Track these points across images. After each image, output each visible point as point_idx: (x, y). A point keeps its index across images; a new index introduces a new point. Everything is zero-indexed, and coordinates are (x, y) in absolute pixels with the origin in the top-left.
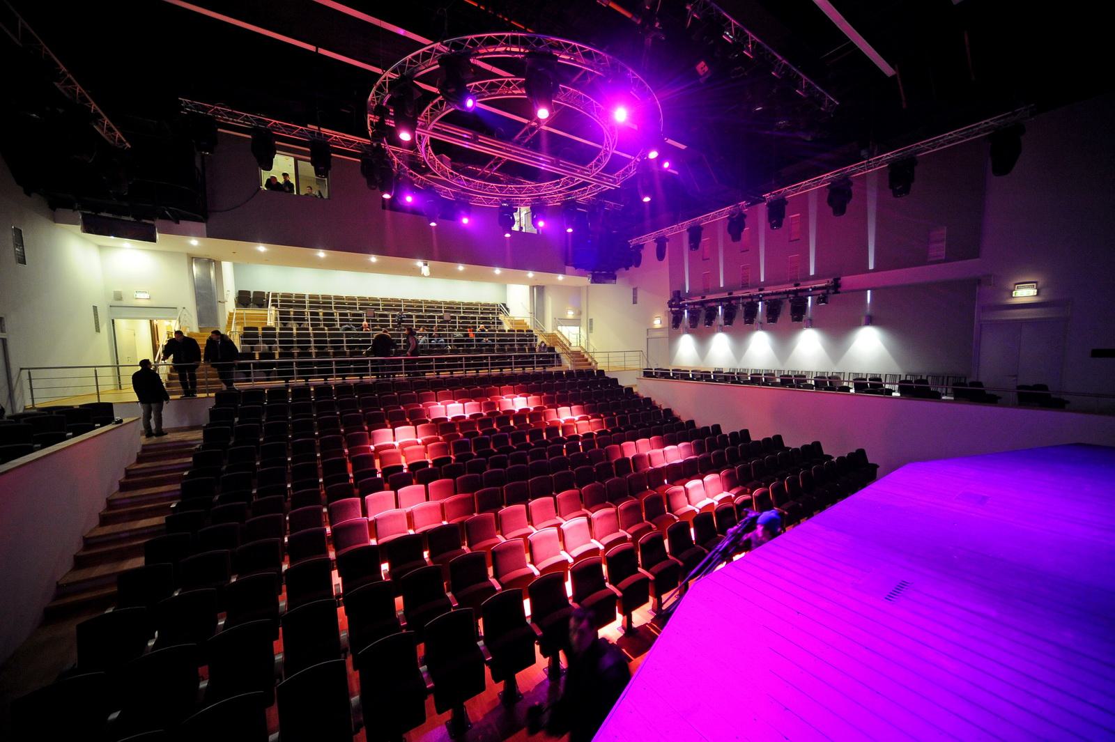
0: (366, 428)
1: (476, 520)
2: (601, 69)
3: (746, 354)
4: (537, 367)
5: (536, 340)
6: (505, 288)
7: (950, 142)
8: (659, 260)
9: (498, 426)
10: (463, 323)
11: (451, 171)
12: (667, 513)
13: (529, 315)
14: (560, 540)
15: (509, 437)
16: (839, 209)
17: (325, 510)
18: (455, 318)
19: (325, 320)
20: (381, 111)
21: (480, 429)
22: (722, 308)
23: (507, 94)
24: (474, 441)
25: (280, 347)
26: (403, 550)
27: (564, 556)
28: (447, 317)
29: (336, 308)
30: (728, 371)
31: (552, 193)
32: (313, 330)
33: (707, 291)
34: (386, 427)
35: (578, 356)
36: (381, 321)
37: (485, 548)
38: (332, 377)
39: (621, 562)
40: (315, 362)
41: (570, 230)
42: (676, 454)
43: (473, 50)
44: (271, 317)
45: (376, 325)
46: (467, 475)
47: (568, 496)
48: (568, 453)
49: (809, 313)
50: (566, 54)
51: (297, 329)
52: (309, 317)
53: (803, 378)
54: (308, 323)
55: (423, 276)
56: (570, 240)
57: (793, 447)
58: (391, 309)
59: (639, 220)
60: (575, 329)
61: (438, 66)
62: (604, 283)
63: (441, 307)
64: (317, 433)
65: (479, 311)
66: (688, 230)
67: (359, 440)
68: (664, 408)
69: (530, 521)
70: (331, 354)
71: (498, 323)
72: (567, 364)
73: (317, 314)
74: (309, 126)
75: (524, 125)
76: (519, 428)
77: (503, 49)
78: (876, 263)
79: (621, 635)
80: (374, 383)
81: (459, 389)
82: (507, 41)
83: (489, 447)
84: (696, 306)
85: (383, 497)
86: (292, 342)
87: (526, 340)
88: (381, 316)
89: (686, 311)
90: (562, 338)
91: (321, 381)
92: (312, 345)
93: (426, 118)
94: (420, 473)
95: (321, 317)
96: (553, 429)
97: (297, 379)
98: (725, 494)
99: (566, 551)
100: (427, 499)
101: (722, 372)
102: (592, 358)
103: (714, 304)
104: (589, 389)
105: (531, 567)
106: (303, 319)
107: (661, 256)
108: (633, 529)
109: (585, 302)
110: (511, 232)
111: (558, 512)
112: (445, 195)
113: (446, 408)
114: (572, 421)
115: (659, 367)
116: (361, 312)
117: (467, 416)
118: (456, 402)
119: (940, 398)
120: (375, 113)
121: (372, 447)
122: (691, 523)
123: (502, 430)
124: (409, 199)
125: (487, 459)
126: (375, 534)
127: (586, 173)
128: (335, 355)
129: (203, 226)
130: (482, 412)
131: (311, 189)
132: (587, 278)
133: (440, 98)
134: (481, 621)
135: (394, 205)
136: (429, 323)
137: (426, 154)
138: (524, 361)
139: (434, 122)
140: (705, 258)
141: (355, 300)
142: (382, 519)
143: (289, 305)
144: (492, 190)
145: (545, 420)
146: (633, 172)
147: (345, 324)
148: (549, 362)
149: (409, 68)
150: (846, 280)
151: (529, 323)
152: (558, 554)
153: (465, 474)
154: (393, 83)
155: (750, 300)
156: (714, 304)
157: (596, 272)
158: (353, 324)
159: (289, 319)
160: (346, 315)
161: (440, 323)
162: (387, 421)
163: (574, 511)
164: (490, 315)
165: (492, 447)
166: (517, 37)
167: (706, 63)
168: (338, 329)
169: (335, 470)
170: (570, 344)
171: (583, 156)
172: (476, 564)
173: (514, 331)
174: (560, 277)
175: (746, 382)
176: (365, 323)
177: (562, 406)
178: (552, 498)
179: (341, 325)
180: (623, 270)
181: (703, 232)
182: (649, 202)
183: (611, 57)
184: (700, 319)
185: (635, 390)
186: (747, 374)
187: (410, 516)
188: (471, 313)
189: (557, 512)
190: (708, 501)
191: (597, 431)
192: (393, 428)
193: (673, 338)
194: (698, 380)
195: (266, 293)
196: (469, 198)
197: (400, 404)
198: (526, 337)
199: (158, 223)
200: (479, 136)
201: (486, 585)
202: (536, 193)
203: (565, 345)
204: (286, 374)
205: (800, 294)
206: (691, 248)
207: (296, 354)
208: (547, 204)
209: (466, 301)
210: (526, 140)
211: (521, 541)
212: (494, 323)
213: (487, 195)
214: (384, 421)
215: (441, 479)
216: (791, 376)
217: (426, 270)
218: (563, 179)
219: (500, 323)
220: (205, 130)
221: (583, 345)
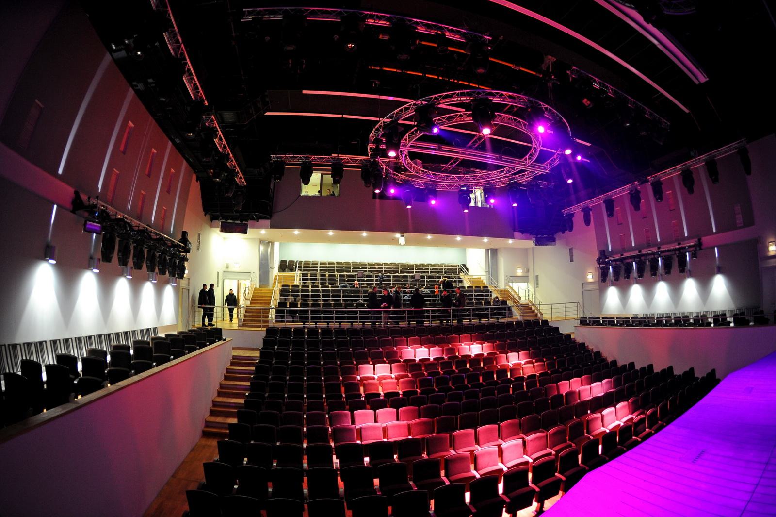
0: (355, 362)
1: (434, 437)
2: (522, 103)
3: (654, 301)
4: (491, 318)
5: (491, 295)
6: (465, 251)
7: (726, 152)
8: (587, 226)
9: (456, 368)
10: (430, 281)
11: (423, 169)
12: (586, 435)
13: (485, 274)
14: (499, 457)
15: (465, 378)
16: (691, 190)
17: (327, 416)
18: (423, 277)
19: (329, 280)
20: (377, 141)
21: (441, 370)
22: (636, 263)
23: (460, 121)
24: (436, 379)
25: (301, 299)
26: (380, 450)
27: (501, 466)
28: (417, 276)
29: (337, 271)
30: (642, 316)
31: (499, 178)
32: (321, 287)
33: (624, 250)
34: (369, 363)
35: (527, 308)
36: (367, 280)
37: (440, 457)
38: (332, 322)
39: (542, 470)
40: (322, 311)
41: (515, 205)
42: (600, 389)
43: (436, 102)
44: (296, 277)
45: (363, 284)
46: (429, 405)
47: (511, 425)
48: (513, 391)
49: (688, 266)
50: (497, 98)
51: (312, 287)
52: (320, 278)
53: (687, 318)
54: (318, 283)
55: (400, 245)
56: (515, 211)
57: (678, 374)
58: (375, 271)
59: (566, 196)
60: (524, 285)
61: (414, 113)
62: (546, 245)
63: (413, 269)
64: (322, 363)
65: (429, 271)
66: (604, 202)
67: (350, 371)
68: (594, 351)
69: (477, 442)
70: (332, 305)
71: (459, 281)
72: (517, 315)
73: (325, 276)
74: (332, 155)
75: (475, 136)
76: (474, 371)
77: (456, 99)
78: (716, 229)
79: (534, 515)
80: (361, 329)
81: (427, 337)
82: (458, 95)
83: (448, 384)
84: (617, 263)
85: (366, 415)
86: (308, 296)
87: (482, 295)
88: (368, 276)
89: (610, 267)
90: (513, 293)
91: (324, 325)
92: (321, 298)
93: (406, 140)
94: (392, 400)
95: (327, 278)
96: (503, 372)
97: (311, 323)
98: (630, 416)
99: (503, 463)
100: (398, 419)
101: (637, 318)
102: (538, 310)
103: (629, 261)
104: (535, 337)
105: (475, 473)
106: (316, 280)
107: (587, 222)
108: (556, 448)
110: (468, 208)
111: (501, 436)
112: (418, 186)
113: (415, 351)
114: (520, 364)
115: (592, 316)
116: (354, 274)
117: (432, 359)
118: (423, 347)
119: (748, 324)
120: (373, 143)
121: (359, 377)
122: (601, 441)
123: (460, 371)
124: (392, 191)
125: (446, 394)
126: (360, 437)
127: (522, 163)
128: (335, 306)
129: (268, 222)
130: (444, 356)
131: (329, 190)
132: (532, 241)
133: (415, 128)
134: (432, 502)
135: (382, 196)
137: (405, 161)
138: (481, 314)
139: (411, 142)
140: (619, 223)
141: (366, 265)
142: (365, 428)
143: (309, 269)
144: (453, 179)
145: (497, 363)
146: (557, 162)
147: (343, 283)
148: (501, 314)
149: (396, 116)
150: (705, 239)
151: (485, 281)
152: (497, 464)
153: (427, 404)
154: (386, 126)
155: (653, 256)
156: (629, 261)
157: (539, 236)
158: (348, 283)
159: (307, 279)
160: (343, 276)
161: (412, 282)
162: (369, 359)
163: (515, 435)
164: (453, 275)
165: (450, 385)
166: (464, 92)
167: (587, 99)
168: (337, 287)
169: (333, 390)
170: (520, 298)
171: (520, 152)
172: (433, 467)
173: (472, 287)
174: (510, 241)
175: (654, 325)
176: (356, 282)
177: (511, 352)
178: (497, 425)
179: (340, 284)
180: (560, 234)
181: (615, 203)
182: (572, 183)
183: (527, 97)
184: (621, 273)
185: (573, 337)
186: (654, 318)
187: (385, 430)
188: (437, 273)
189: (499, 436)
190: (617, 423)
191: (539, 372)
192: (374, 364)
193: (602, 290)
194: (621, 325)
195: (295, 261)
196: (436, 186)
197: (379, 347)
198: (483, 292)
199: (250, 223)
200: (442, 146)
201: (438, 480)
202: (486, 179)
203: (516, 299)
204: (304, 319)
205: (682, 251)
206: (608, 216)
207: (310, 305)
208: (495, 186)
209: (433, 263)
210: (476, 146)
211: (469, 454)
212: (455, 281)
213: (448, 182)
215: (409, 406)
216: (680, 317)
217: (402, 240)
218: (506, 168)
219: (461, 281)
220: (279, 169)
221: (531, 298)
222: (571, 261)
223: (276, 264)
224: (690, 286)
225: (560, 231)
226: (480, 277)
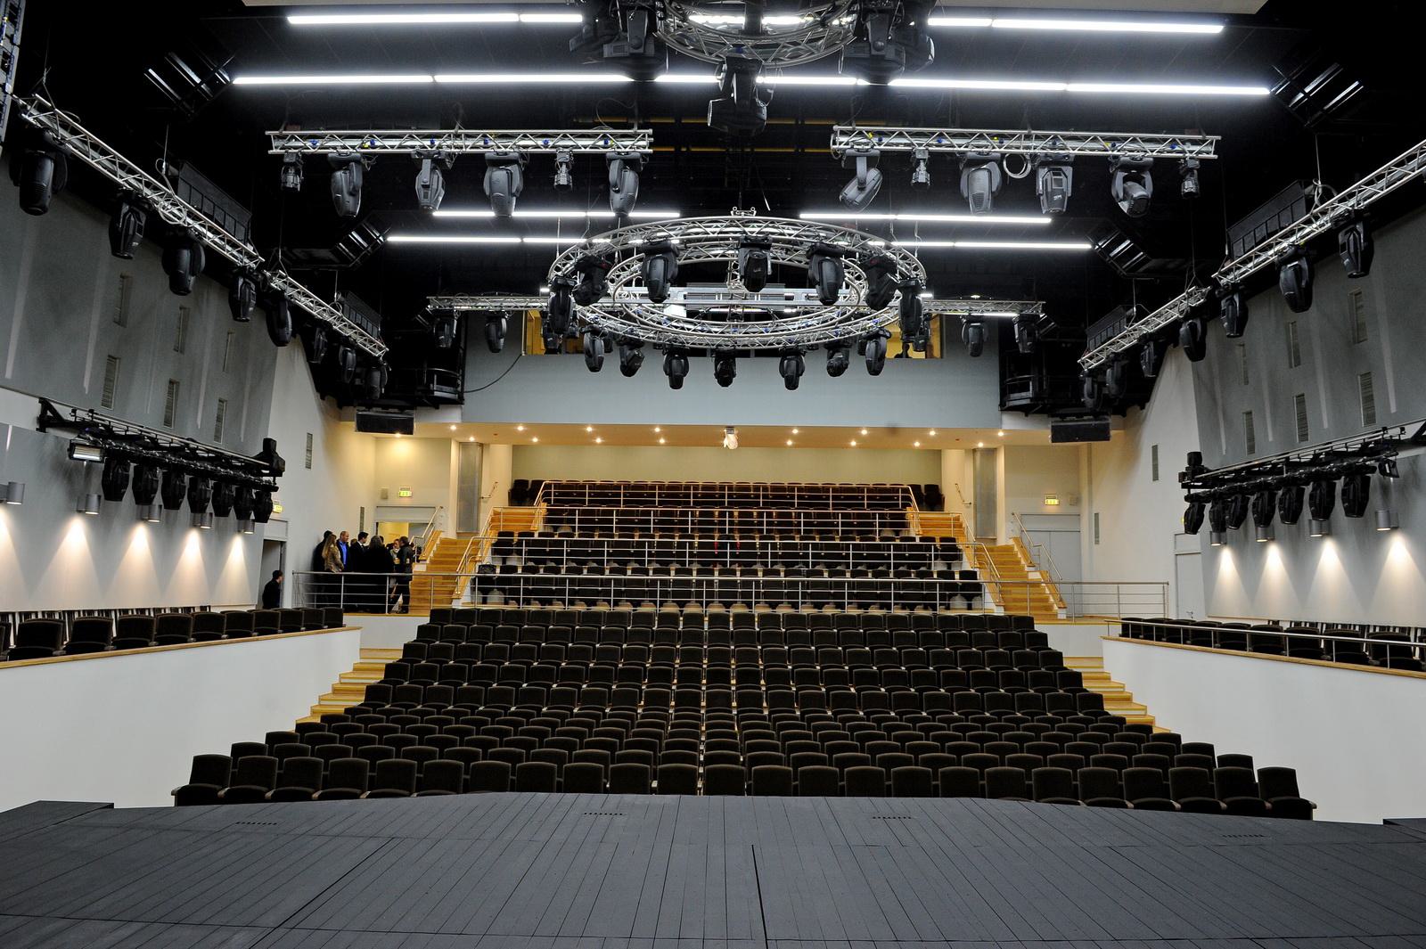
36: (860, 524)
136: (598, 523)
222: (1154, 480)
225: (1133, 404)
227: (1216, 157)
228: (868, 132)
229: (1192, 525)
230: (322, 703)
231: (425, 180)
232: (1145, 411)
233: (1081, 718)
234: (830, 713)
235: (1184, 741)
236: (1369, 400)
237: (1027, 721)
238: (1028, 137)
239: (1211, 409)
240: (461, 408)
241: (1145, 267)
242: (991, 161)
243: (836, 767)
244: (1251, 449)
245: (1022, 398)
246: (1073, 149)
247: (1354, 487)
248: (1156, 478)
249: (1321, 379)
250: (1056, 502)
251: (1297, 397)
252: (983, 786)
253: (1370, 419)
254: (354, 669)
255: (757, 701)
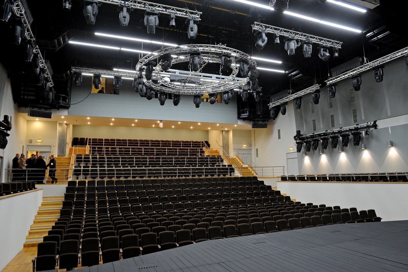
86: (97, 161)
109: (254, 140)
141: (149, 141)
159: (95, 151)
198: (216, 159)
209: (185, 140)
214: (95, 191)
223: (69, 140)
224: (366, 155)
226: (216, 149)
227: (341, 48)
228: (263, 25)
229: (299, 150)
230: (36, 218)
231: (125, 15)
232: (275, 120)
233: (241, 207)
234: (132, 213)
235: (327, 206)
236: (355, 116)
237: (188, 212)
238: (302, 35)
239: (300, 119)
240: (68, 110)
241: (299, 79)
242: (295, 40)
243: (274, 221)
244: (315, 130)
245: (245, 115)
246: (314, 41)
247: (357, 138)
248: (279, 138)
249: (339, 112)
250: (245, 146)
251: (331, 116)
252: (322, 220)
253: (355, 121)
254: (42, 205)
255: (105, 211)
